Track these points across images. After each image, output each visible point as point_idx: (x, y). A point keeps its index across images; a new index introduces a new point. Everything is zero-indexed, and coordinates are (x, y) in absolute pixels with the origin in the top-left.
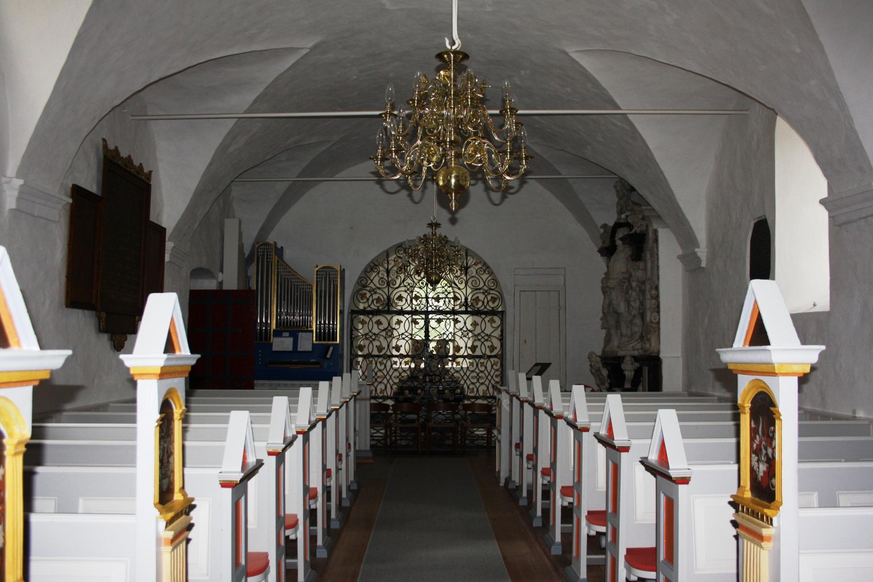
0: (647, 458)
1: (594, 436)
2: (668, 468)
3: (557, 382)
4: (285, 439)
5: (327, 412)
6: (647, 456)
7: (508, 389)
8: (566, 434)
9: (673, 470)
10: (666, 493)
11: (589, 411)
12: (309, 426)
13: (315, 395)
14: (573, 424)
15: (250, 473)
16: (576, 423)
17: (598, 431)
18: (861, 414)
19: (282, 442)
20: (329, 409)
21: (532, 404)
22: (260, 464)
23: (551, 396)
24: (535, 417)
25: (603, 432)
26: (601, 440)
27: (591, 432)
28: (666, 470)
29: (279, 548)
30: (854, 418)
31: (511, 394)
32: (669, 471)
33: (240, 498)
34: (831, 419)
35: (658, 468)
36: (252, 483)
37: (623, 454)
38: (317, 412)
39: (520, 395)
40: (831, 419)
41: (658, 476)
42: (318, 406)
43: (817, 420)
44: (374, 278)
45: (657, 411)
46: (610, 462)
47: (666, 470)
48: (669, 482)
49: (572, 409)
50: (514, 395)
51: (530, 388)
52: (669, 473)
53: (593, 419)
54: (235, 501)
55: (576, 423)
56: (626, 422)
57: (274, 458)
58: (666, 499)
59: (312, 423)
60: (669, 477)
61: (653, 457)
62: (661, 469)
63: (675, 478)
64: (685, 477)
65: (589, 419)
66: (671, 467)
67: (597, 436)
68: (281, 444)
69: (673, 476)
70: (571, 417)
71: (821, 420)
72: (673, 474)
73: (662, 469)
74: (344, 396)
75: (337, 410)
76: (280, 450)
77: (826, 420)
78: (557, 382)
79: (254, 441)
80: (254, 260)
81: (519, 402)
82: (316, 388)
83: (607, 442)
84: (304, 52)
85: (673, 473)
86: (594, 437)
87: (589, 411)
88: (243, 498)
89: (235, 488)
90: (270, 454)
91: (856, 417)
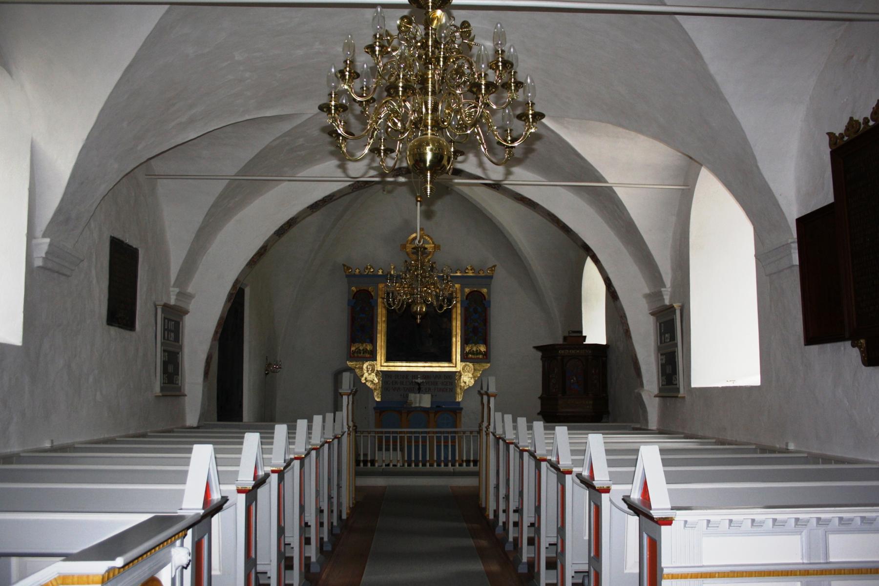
0: (629, 496)
1: (623, 499)
2: (650, 508)
3: (525, 419)
4: (285, 461)
5: (284, 462)
6: (629, 494)
7: (517, 441)
8: (548, 477)
9: (655, 509)
10: (650, 534)
11: (572, 455)
12: (285, 464)
13: (310, 428)
14: (556, 466)
15: (260, 482)
16: (594, 482)
17: (629, 494)
18: (792, 447)
19: (252, 479)
20: (287, 458)
21: (532, 454)
22: (267, 476)
23: (591, 457)
24: (521, 460)
25: (586, 473)
26: (634, 509)
27: (574, 474)
28: (648, 510)
29: (548, 214)
30: (787, 451)
31: (521, 448)
32: (651, 512)
33: (203, 537)
34: (777, 452)
35: (640, 507)
36: (260, 491)
37: (664, 529)
38: (273, 462)
39: (519, 443)
40: (777, 452)
41: (641, 516)
42: (313, 436)
43: (818, 463)
44: (486, 504)
45: (532, 423)
46: (645, 536)
47: (648, 510)
48: (594, 490)
49: (554, 452)
50: (500, 438)
51: (515, 428)
52: (651, 514)
53: (576, 463)
54: (196, 539)
55: (594, 482)
56: (667, 483)
57: (243, 496)
58: (649, 540)
59: (287, 462)
60: (651, 518)
61: (636, 496)
62: (643, 509)
63: (598, 487)
64: (668, 518)
65: (610, 477)
66: (653, 507)
67: (579, 476)
68: (251, 481)
69: (654, 517)
70: (554, 459)
71: (823, 463)
72: (656, 514)
73: (644, 509)
74: (326, 436)
75: (302, 460)
76: (250, 487)
77: (724, 445)
78: (525, 419)
79: (219, 484)
80: (644, 506)
81: (533, 463)
82: (310, 421)
83: (587, 483)
84: (310, 116)
85: (655, 514)
86: (623, 502)
87: (572, 455)
88: (254, 504)
89: (248, 494)
90: (240, 491)
91: (788, 449)
